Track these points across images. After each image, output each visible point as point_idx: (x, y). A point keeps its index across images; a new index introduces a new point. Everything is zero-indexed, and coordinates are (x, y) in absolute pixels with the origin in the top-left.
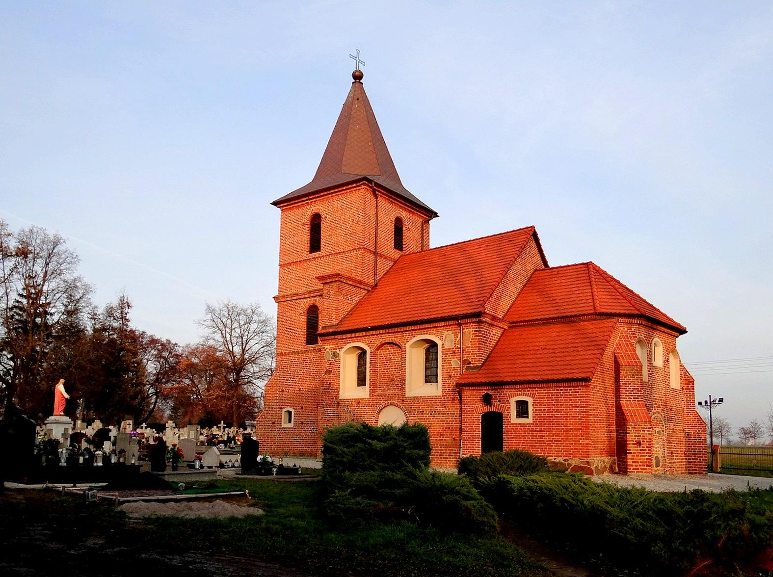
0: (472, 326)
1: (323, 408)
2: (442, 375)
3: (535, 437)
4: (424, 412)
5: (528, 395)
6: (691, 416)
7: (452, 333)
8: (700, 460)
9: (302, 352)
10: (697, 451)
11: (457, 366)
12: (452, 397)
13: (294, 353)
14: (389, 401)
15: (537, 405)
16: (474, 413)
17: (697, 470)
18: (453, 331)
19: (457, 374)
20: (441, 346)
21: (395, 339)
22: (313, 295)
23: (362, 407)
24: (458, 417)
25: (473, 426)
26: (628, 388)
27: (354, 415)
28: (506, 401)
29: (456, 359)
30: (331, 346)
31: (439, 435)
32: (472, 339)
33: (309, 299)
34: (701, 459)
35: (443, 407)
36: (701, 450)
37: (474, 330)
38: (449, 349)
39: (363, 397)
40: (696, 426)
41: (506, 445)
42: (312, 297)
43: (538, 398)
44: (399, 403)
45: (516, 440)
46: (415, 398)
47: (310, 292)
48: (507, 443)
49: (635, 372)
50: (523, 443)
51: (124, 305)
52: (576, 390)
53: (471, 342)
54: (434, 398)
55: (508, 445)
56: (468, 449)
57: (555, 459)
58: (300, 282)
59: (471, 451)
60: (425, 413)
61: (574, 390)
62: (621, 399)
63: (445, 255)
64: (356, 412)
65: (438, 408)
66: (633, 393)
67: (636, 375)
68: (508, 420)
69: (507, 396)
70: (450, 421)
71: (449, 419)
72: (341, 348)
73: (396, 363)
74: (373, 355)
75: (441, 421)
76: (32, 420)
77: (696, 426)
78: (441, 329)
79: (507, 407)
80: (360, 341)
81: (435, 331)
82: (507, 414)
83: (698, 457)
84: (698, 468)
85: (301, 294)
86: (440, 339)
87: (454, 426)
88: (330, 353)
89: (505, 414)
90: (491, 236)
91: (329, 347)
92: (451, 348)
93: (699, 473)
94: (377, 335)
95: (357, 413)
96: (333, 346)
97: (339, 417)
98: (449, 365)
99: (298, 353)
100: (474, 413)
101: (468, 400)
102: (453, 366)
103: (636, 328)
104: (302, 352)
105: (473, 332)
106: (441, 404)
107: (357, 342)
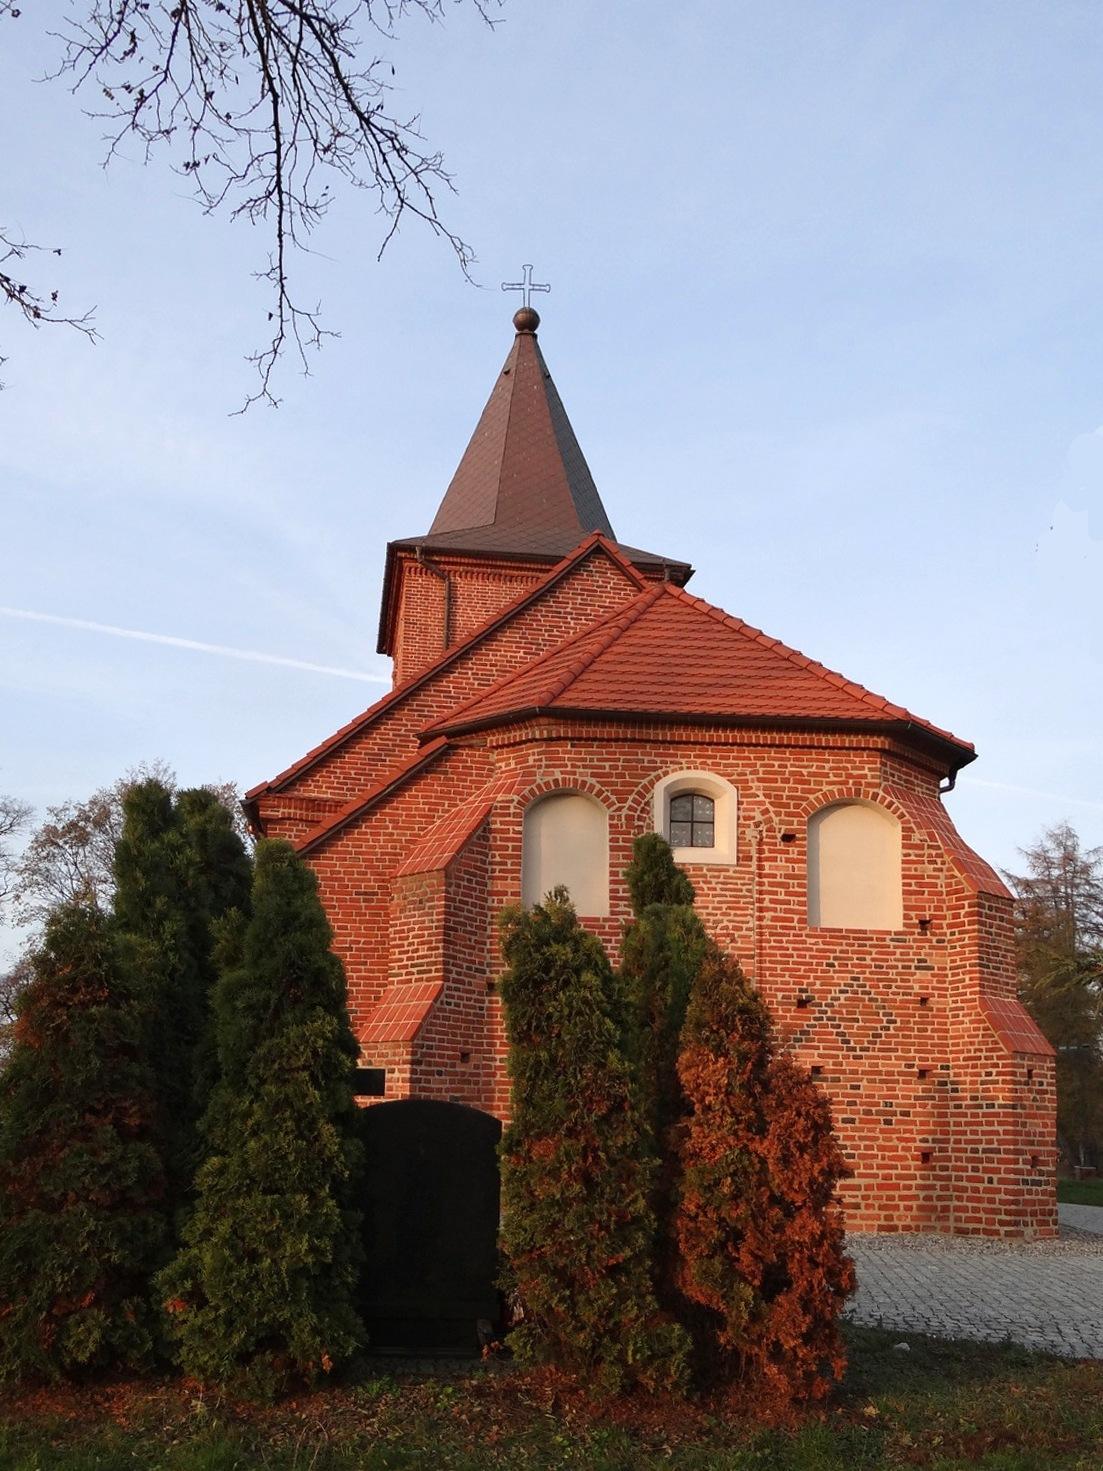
6: (966, 1019)
8: (990, 1181)
10: (980, 1147)
17: (979, 1220)
26: (406, 943)
34: (995, 1177)
36: (995, 1146)
40: (979, 1058)
49: (425, 893)
51: (560, 892)
66: (419, 958)
67: (428, 901)
77: (979, 1058)
83: (986, 1170)
84: (986, 1211)
93: (986, 1232)
103: (539, 754)
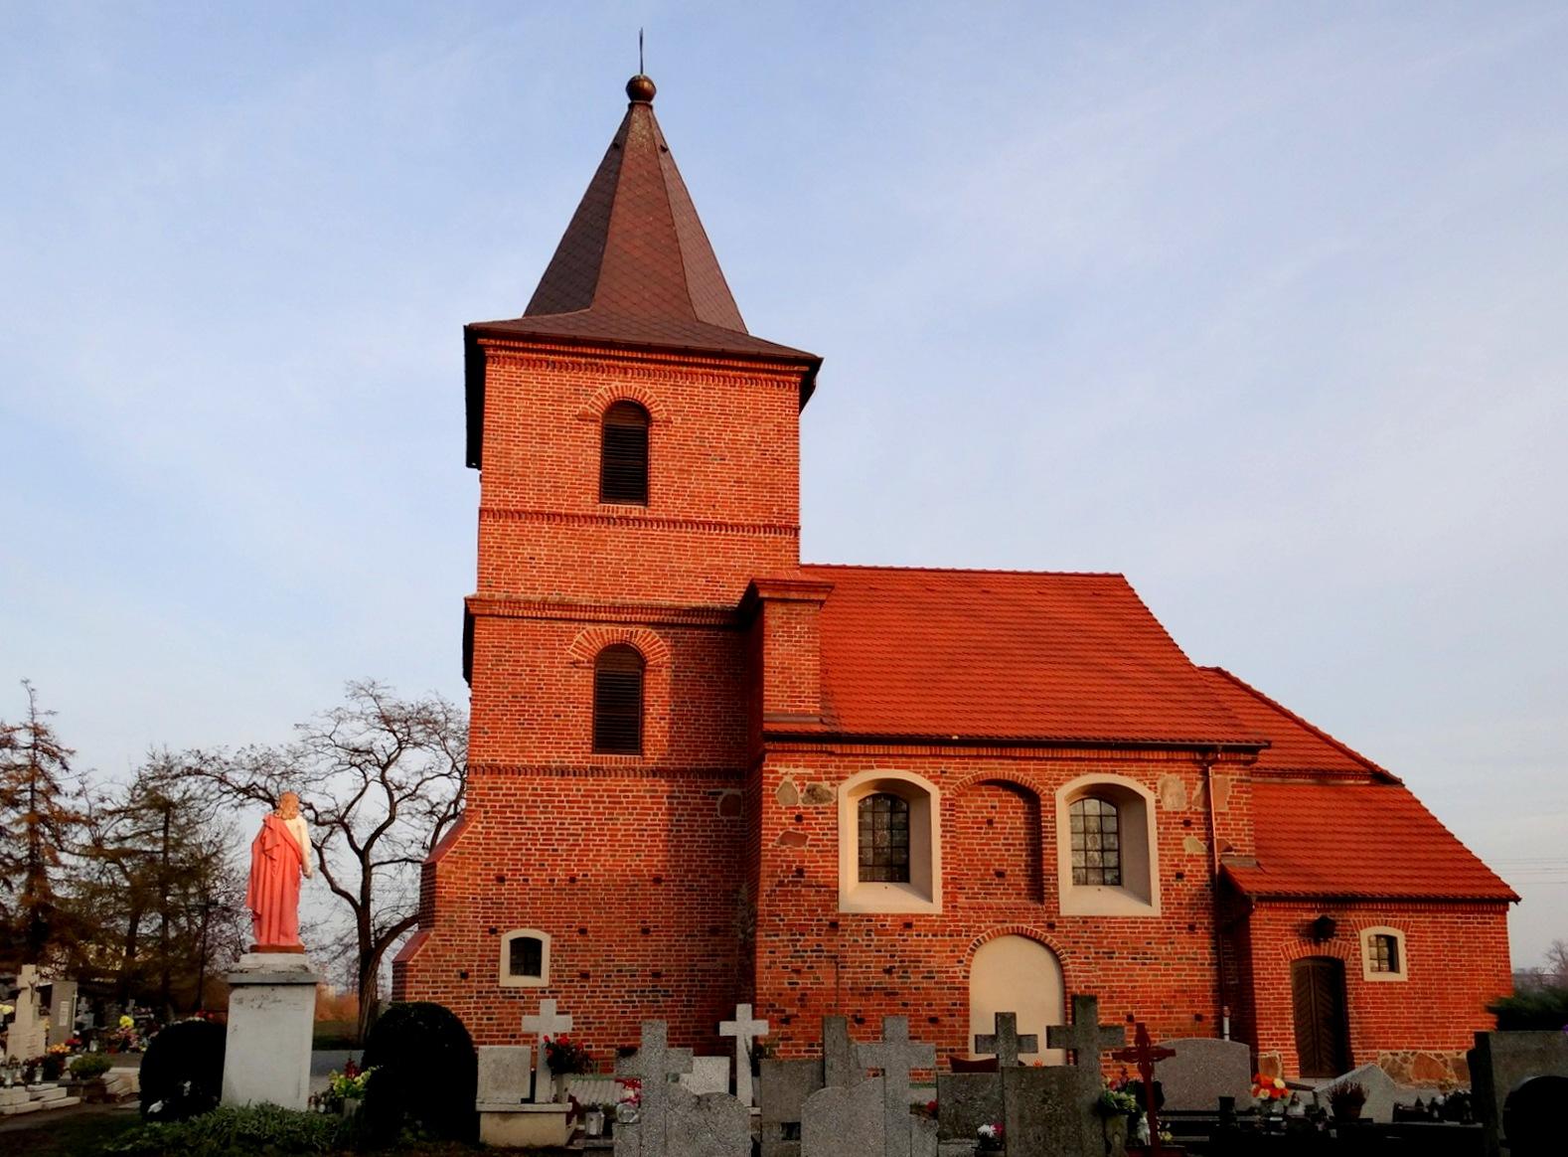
0: (1229, 769)
1: (777, 935)
2: (1161, 870)
3: (1414, 1011)
4: (1114, 953)
5: (1395, 925)
7: (1181, 779)
9: (578, 772)
11: (1198, 853)
12: (1187, 921)
13: (546, 770)
14: (1007, 925)
15: (1414, 946)
16: (1281, 959)
18: (1183, 775)
19: (1200, 871)
20: (1154, 804)
21: (1022, 774)
24: (1206, 966)
25: (1281, 987)
28: (1351, 935)
29: (1196, 838)
30: (800, 770)
31: (1159, 1007)
32: (1231, 797)
33: (604, 627)
35: (1166, 944)
37: (1235, 777)
38: (1175, 813)
41: (1356, 1028)
42: (620, 623)
43: (1416, 932)
44: (1039, 930)
45: (1376, 1018)
46: (1085, 920)
48: (1357, 1023)
50: (1391, 1023)
52: (1485, 918)
53: (1229, 803)
54: (1141, 923)
55: (1361, 1028)
56: (1271, 1039)
57: (1458, 1054)
58: (570, 574)
59: (1279, 1043)
60: (1117, 955)
61: (1481, 918)
62: (436, 918)
65: (1153, 945)
68: (1357, 974)
69: (1350, 926)
70: (1186, 975)
71: (1184, 970)
72: (839, 778)
73: (1007, 831)
74: (950, 806)
75: (1162, 975)
76: (96, 980)
78: (1150, 768)
79: (1353, 947)
81: (1135, 768)
82: (1353, 962)
85: (584, 608)
86: (1150, 788)
87: (1197, 986)
88: (798, 789)
89: (1349, 964)
92: (1180, 810)
94: (963, 757)
96: (811, 771)
97: (837, 961)
98: (1177, 850)
99: (563, 772)
100: (1281, 959)
101: (1264, 929)
102: (1186, 853)
104: (578, 772)
105: (1235, 783)
106: (1159, 936)
107: (896, 768)
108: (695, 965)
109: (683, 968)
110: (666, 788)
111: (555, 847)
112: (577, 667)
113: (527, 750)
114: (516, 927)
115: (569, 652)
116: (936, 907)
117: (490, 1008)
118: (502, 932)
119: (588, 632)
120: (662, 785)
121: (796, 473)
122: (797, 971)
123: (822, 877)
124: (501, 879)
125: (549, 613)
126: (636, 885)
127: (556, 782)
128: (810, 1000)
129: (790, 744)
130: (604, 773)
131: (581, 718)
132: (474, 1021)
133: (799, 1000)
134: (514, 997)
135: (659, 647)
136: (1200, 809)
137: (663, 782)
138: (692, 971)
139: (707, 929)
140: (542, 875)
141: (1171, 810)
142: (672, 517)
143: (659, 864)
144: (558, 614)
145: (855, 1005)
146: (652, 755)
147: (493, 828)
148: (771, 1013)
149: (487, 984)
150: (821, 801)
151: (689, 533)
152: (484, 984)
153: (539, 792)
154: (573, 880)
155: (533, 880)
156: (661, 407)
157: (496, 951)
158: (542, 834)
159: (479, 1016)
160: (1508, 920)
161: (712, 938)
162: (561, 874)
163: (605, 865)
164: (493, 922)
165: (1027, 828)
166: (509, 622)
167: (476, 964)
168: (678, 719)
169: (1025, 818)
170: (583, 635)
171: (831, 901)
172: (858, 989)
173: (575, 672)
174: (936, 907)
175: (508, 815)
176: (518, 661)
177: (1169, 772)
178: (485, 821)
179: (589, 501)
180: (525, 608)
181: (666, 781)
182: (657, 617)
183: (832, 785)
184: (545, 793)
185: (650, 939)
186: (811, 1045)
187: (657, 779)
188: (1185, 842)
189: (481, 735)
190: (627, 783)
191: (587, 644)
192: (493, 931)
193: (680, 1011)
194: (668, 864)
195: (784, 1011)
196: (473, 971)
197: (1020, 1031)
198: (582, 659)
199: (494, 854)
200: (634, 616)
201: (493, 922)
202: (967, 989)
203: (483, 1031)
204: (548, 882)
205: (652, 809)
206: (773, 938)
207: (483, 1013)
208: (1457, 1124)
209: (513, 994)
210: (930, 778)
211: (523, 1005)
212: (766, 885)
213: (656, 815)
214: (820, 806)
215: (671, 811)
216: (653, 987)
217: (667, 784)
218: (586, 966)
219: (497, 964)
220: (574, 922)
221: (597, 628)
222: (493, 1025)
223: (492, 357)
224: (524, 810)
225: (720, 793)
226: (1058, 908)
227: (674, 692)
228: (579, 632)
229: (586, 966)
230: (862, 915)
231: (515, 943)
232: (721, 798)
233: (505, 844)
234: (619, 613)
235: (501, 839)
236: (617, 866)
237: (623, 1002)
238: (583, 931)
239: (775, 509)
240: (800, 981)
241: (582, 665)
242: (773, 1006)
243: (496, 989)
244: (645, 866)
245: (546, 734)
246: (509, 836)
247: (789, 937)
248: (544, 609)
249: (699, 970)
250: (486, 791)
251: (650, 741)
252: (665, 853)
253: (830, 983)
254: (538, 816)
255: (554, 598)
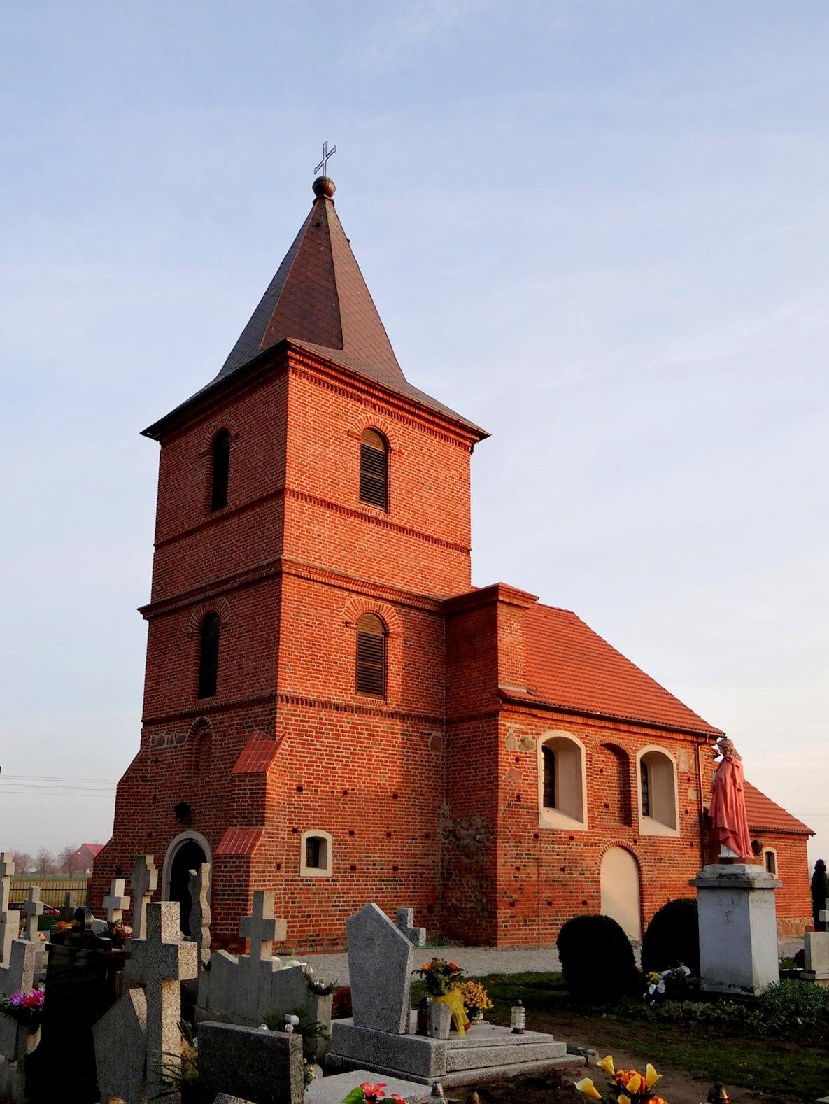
1: (508, 842)
22: (378, 593)
23: (577, 845)
27: (565, 859)
30: (518, 726)
33: (364, 599)
39: (580, 829)
47: (376, 587)
58: (343, 553)
63: (572, 624)
64: (568, 854)
72: (538, 734)
80: (570, 731)
85: (355, 582)
88: (516, 738)
90: (569, 612)
91: (513, 725)
92: (685, 771)
95: (570, 856)
96: (523, 727)
97: (538, 861)
99: (338, 708)
107: (565, 730)
108: (417, 861)
109: (383, 863)
110: (400, 727)
111: (335, 766)
112: (347, 627)
113: (316, 687)
114: (310, 828)
115: (342, 613)
116: (584, 827)
117: (293, 893)
118: (301, 832)
119: (353, 600)
120: (398, 725)
121: (468, 510)
122: (518, 869)
123: (530, 802)
124: (300, 789)
125: (333, 582)
126: (383, 799)
127: (334, 714)
128: (525, 889)
129: (516, 707)
130: (363, 711)
131: (349, 664)
132: (283, 904)
133: (520, 889)
134: (310, 885)
135: (395, 620)
136: (694, 772)
137: (398, 723)
138: (416, 865)
139: (423, 834)
140: (326, 787)
141: (683, 771)
142: (403, 524)
143: (397, 784)
144: (338, 583)
145: (547, 893)
146: (393, 703)
147: (295, 747)
148: (505, 898)
149: (292, 874)
150: (528, 748)
151: (413, 539)
152: (290, 874)
153: (324, 721)
154: (345, 793)
155: (321, 791)
156: (396, 441)
157: (297, 847)
158: (327, 755)
159: (286, 900)
160: (807, 845)
161: (427, 841)
162: (338, 788)
163: (365, 783)
164: (296, 823)
165: (618, 777)
166: (304, 583)
167: (284, 857)
168: (407, 676)
169: (617, 770)
170: (351, 602)
171: (534, 819)
172: (549, 881)
173: (346, 630)
174: (584, 827)
175: (305, 737)
176: (311, 615)
177: (682, 748)
178: (289, 741)
179: (353, 501)
180: (319, 574)
181: (400, 722)
182: (398, 598)
183: (534, 738)
184: (328, 722)
185: (391, 840)
186: (526, 921)
187: (394, 719)
188: (689, 791)
189: (286, 670)
190: (377, 720)
191: (353, 610)
192: (295, 831)
193: (409, 896)
194: (402, 784)
195: (511, 897)
196: (282, 863)
197: (129, 898)
198: (350, 621)
199: (296, 768)
200: (385, 594)
201: (296, 823)
202: (599, 882)
203: (289, 912)
204: (330, 793)
205: (392, 742)
206: (506, 844)
207: (289, 898)
208: (118, 950)
209: (309, 883)
210: (581, 739)
211: (315, 891)
212: (502, 807)
213: (394, 746)
214: (527, 752)
215: (403, 745)
216: (394, 877)
217: (400, 724)
218: (354, 861)
219: (299, 857)
220: (346, 826)
221: (360, 598)
222: (296, 907)
223: (292, 368)
224: (314, 734)
225: (430, 734)
226: (638, 830)
227: (405, 655)
228: (348, 600)
229: (354, 861)
230: (550, 830)
231: (309, 840)
232: (431, 738)
233: (303, 761)
234: (376, 590)
235: (300, 756)
236: (372, 783)
237: (376, 889)
238: (352, 833)
239: (459, 533)
240: (520, 876)
241: (351, 625)
242: (506, 893)
243: (297, 878)
244: (389, 785)
245: (328, 675)
246: (305, 755)
247: (514, 844)
248: (331, 577)
249: (419, 865)
250: (289, 717)
251: (390, 690)
252: (400, 776)
253: (534, 877)
254: (323, 740)
255: (338, 570)
